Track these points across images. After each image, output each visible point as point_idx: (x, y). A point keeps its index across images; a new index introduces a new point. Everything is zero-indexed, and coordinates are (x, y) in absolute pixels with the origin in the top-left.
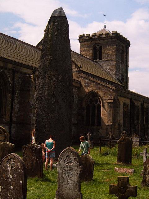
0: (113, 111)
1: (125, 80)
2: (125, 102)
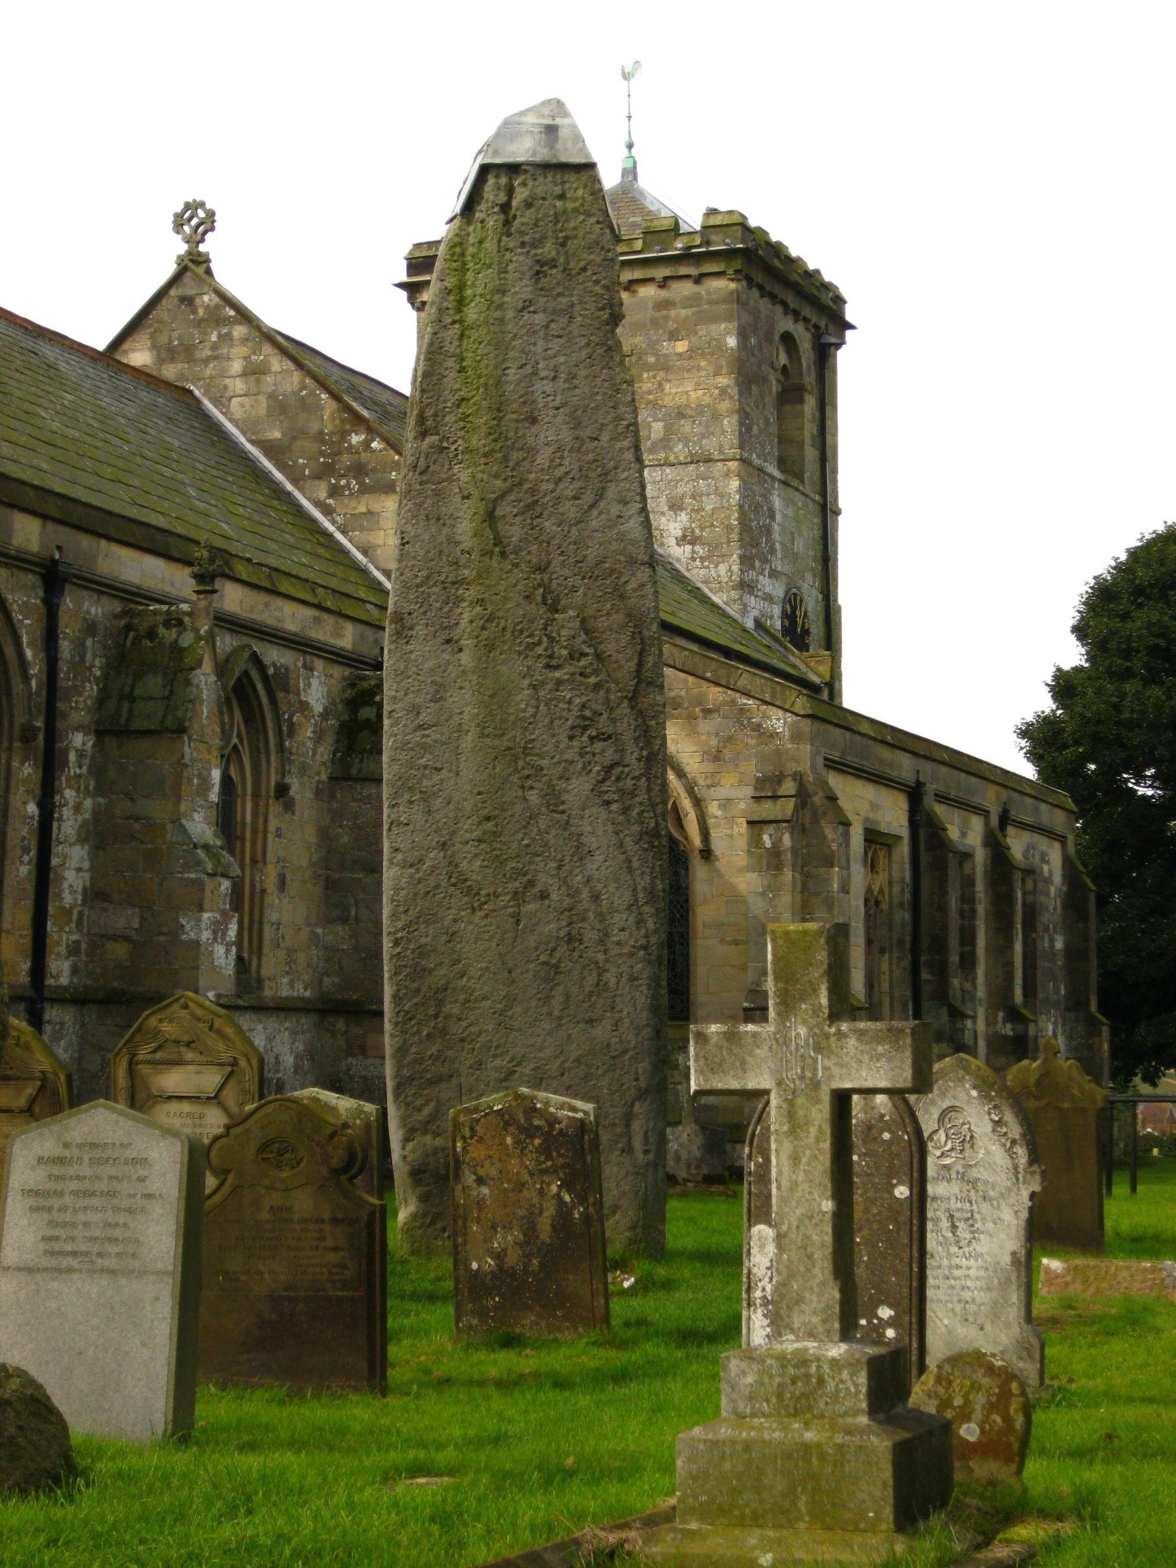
0: (798, 897)
1: (811, 625)
2: (872, 816)
